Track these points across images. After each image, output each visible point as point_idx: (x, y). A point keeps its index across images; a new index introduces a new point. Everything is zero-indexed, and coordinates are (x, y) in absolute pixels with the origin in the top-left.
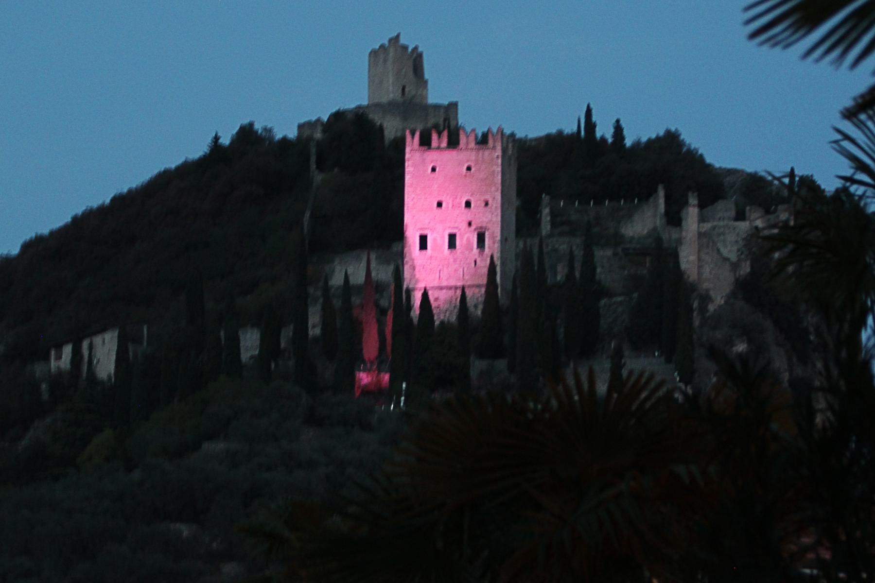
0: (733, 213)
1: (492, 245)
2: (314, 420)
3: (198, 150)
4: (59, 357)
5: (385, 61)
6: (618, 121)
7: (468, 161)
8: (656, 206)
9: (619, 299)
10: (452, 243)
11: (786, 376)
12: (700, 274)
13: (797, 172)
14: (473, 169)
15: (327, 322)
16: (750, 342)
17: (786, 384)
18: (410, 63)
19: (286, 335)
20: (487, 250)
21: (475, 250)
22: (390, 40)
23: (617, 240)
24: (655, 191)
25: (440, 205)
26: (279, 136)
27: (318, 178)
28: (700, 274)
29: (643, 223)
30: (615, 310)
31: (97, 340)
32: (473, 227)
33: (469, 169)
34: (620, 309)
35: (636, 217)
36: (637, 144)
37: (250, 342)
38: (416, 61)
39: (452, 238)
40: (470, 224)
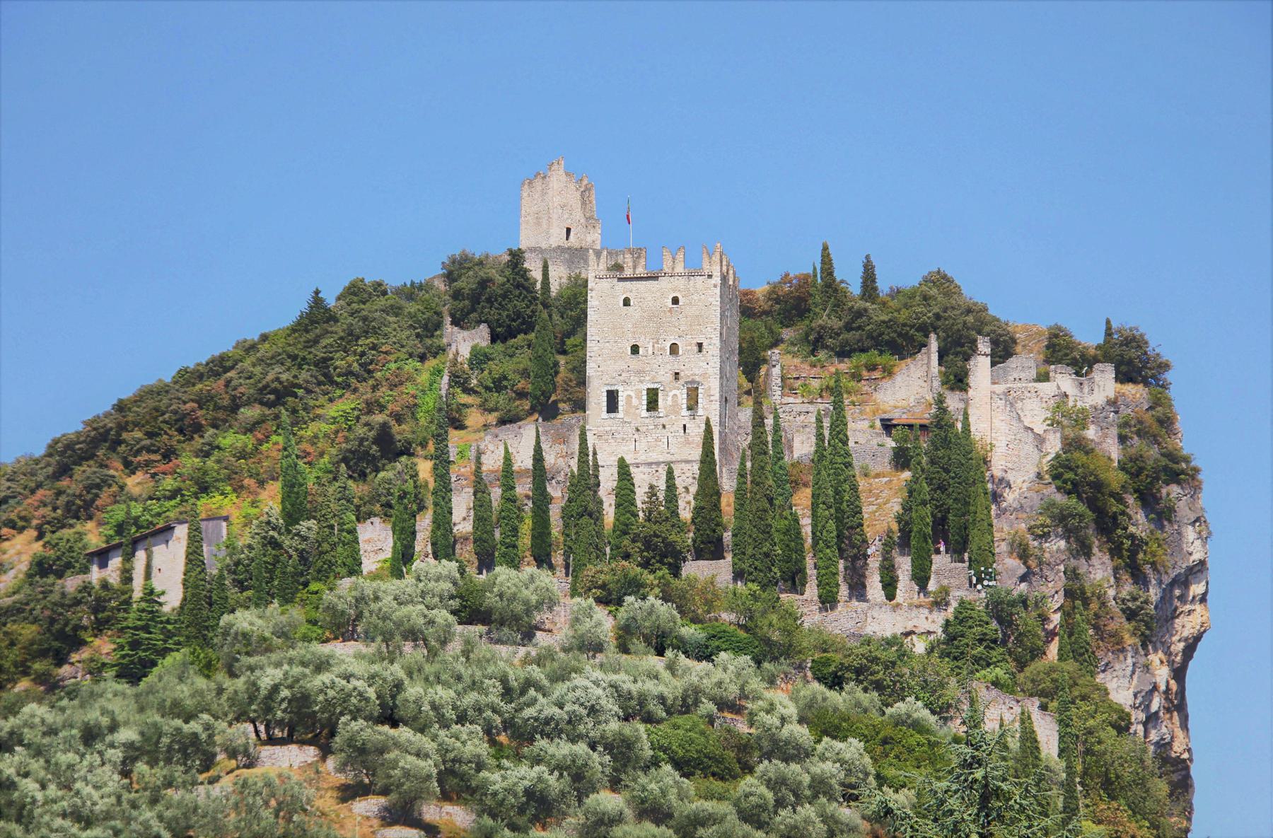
1: (710, 407)
6: (867, 257)
7: (674, 291)
10: (652, 404)
13: (1114, 325)
20: (700, 412)
21: (685, 412)
25: (635, 349)
32: (681, 381)
36: (896, 293)
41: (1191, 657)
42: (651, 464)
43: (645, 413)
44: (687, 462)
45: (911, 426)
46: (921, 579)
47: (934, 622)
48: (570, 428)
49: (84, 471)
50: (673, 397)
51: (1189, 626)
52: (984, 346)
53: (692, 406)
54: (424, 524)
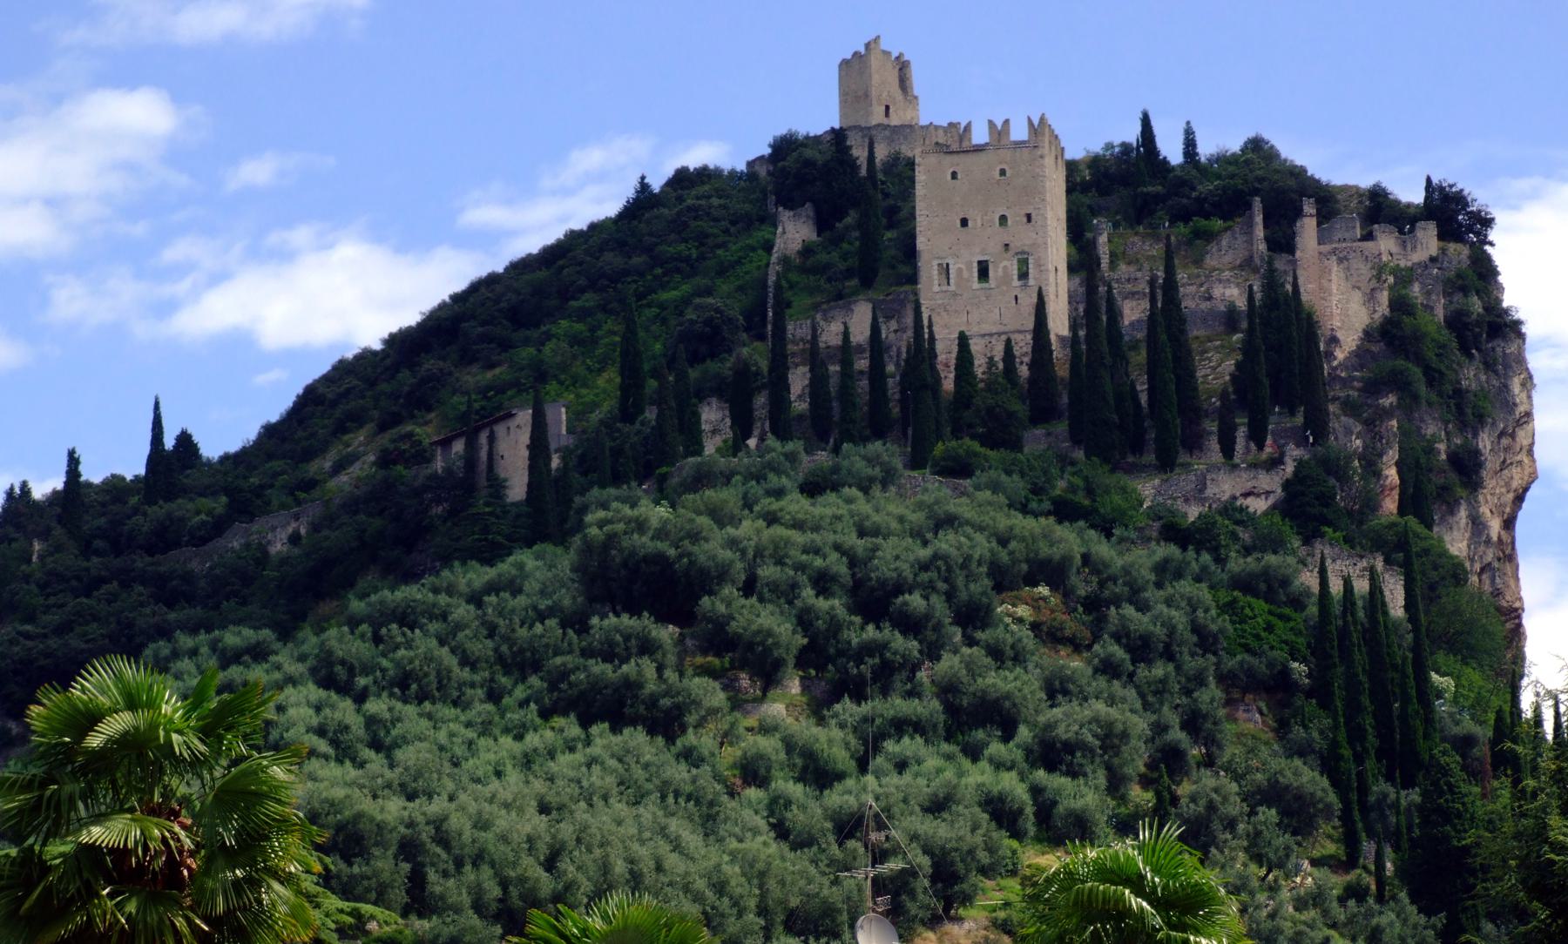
8: (1250, 225)
13: (1435, 181)
14: (1008, 173)
17: (1444, 457)
20: (1031, 282)
21: (1016, 283)
25: (964, 222)
30: (1215, 369)
32: (1011, 252)
33: (1003, 172)
41: (1520, 508)
42: (984, 336)
43: (976, 285)
44: (1020, 332)
45: (1519, 499)
46: (1257, 437)
47: (1271, 482)
48: (902, 303)
49: (430, 364)
50: (1005, 267)
51: (1517, 477)
52: (1309, 207)
53: (1023, 275)
54: (761, 401)
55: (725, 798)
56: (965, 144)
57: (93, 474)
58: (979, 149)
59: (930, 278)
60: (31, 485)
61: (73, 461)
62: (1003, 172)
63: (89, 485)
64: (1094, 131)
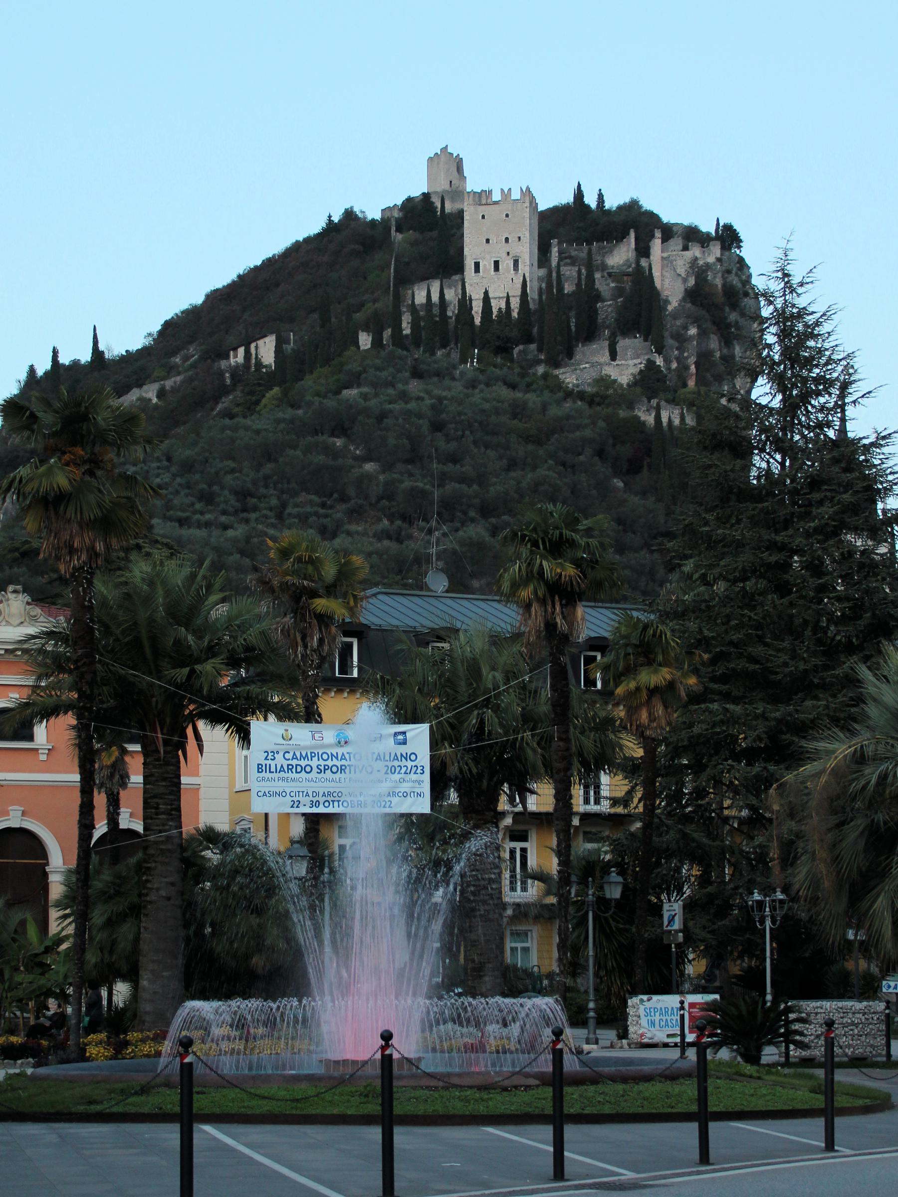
0: (681, 247)
1: (525, 268)
2: (417, 374)
3: (315, 227)
4: (236, 356)
5: (438, 164)
8: (629, 245)
9: (609, 303)
11: (718, 354)
12: (662, 285)
15: (414, 325)
16: (699, 327)
18: (455, 164)
19: (387, 333)
21: (512, 272)
22: (441, 150)
23: (604, 267)
24: (628, 234)
25: (488, 241)
26: (370, 218)
27: (399, 237)
28: (662, 285)
29: (621, 255)
30: (607, 309)
31: (261, 343)
32: (511, 256)
33: (507, 216)
34: (609, 310)
35: (615, 252)
37: (365, 340)
38: (459, 164)
39: (496, 264)
40: (508, 253)
43: (492, 273)
50: (507, 264)
52: (658, 234)
55: (158, 464)
56: (489, 201)
57: (65, 359)
58: (496, 203)
59: (470, 269)
60: (36, 367)
61: (55, 353)
62: (507, 216)
63: (63, 365)
64: (554, 195)
